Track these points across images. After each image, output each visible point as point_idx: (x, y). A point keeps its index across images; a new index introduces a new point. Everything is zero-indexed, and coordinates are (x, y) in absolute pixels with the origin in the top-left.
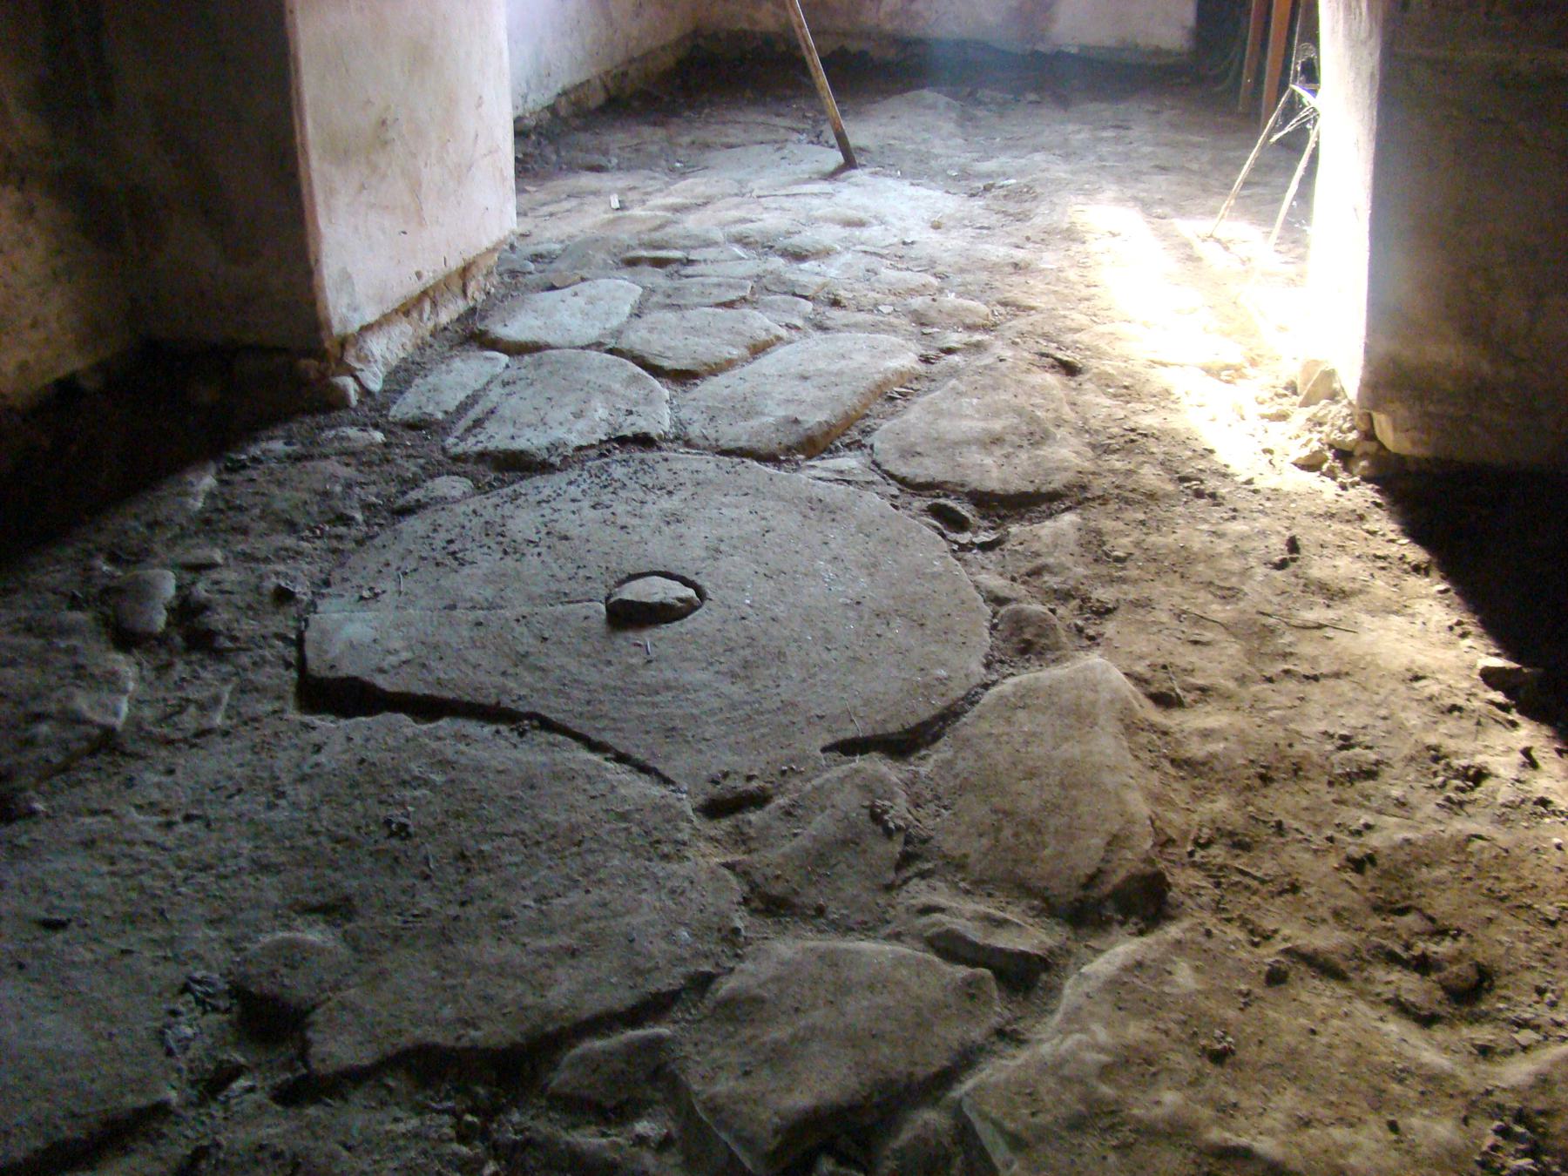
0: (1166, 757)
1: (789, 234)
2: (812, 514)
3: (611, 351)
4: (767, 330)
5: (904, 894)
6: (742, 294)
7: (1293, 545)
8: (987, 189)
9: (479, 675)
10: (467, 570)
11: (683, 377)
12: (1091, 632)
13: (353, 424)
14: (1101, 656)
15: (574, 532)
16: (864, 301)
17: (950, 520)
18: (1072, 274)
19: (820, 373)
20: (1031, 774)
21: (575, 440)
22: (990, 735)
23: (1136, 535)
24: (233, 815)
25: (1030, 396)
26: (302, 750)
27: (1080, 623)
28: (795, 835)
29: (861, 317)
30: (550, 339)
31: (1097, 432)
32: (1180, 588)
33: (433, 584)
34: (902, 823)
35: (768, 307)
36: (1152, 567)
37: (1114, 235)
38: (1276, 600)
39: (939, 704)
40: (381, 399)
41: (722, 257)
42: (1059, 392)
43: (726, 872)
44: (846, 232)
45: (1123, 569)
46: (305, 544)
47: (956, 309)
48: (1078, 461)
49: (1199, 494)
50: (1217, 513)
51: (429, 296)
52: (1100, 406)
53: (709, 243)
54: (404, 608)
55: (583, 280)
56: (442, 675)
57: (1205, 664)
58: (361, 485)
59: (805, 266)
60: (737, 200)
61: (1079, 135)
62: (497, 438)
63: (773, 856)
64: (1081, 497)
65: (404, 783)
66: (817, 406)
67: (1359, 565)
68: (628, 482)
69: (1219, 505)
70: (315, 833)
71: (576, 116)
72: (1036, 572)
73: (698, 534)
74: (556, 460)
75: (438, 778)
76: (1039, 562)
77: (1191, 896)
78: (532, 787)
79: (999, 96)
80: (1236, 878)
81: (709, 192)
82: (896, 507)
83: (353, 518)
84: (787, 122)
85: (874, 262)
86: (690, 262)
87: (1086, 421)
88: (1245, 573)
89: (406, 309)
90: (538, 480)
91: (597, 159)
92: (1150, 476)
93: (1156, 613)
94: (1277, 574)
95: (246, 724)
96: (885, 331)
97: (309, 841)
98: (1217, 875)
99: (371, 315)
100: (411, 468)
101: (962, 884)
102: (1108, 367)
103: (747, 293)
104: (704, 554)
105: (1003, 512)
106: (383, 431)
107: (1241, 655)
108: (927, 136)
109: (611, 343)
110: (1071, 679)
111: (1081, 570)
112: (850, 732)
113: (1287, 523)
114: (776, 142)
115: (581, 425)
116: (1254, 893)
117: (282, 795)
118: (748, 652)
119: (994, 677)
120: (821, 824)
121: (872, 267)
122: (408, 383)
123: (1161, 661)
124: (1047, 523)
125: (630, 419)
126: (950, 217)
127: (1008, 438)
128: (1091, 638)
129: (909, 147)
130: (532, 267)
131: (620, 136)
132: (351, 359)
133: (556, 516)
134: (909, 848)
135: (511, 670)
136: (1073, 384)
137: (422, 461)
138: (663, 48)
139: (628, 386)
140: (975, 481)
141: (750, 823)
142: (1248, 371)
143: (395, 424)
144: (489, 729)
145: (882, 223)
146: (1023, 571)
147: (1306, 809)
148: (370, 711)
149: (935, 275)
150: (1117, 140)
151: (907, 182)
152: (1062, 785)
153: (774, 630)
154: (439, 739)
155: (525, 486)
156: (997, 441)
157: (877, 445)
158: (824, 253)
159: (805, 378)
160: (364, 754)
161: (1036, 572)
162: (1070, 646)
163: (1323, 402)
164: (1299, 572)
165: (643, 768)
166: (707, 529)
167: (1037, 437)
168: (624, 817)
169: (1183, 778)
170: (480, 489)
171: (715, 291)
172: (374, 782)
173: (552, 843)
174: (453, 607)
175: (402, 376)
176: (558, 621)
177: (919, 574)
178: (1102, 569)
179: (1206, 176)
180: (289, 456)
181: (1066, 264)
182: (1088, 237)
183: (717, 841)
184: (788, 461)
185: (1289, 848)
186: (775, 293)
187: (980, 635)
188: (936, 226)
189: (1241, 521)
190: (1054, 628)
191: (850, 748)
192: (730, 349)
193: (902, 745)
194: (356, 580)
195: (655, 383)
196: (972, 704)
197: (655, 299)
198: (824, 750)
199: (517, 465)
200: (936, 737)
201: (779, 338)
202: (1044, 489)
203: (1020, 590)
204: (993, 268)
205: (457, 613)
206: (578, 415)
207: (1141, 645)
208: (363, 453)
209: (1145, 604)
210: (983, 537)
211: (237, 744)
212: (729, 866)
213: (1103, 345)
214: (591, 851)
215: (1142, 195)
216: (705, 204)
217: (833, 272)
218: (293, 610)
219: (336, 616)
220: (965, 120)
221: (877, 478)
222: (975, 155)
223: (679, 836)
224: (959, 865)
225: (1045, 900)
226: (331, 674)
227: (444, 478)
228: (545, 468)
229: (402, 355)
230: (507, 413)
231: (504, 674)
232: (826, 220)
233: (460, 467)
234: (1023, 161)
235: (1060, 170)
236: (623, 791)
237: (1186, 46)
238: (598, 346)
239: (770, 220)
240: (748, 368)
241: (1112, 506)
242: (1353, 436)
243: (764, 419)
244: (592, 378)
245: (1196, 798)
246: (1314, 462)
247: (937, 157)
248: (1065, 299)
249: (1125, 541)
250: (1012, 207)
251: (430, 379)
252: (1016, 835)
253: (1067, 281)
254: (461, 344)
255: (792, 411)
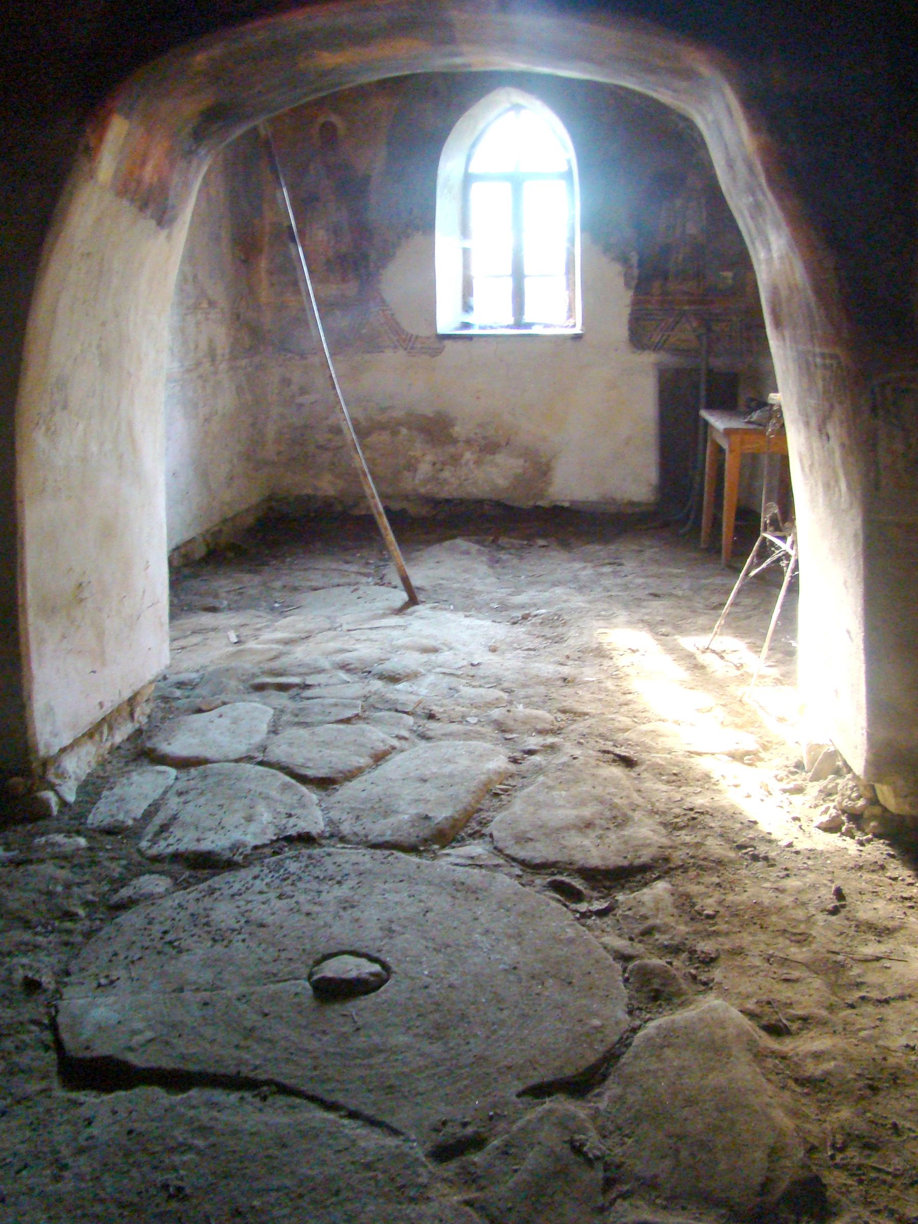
0: (790, 1077)
1: (381, 661)
2: (459, 895)
3: (261, 763)
4: (383, 741)
5: (613, 1214)
6: (356, 712)
7: (839, 894)
8: (525, 617)
9: (215, 1049)
10: (185, 957)
11: (325, 783)
12: (703, 978)
13: (59, 831)
14: (717, 998)
15: (269, 920)
16: (453, 715)
17: (570, 894)
18: (609, 684)
19: (435, 776)
20: (690, 1102)
21: (252, 841)
22: (648, 1071)
23: (717, 895)
24: (24, 1189)
25: (605, 787)
26: (76, 1124)
27: (693, 971)
28: (516, 1171)
29: (454, 727)
30: (209, 754)
31: (664, 813)
32: (763, 937)
33: (158, 971)
34: (598, 1153)
35: (379, 722)
36: (736, 920)
37: (634, 651)
38: (838, 940)
39: (601, 1048)
40: (77, 809)
41: (332, 681)
42: (626, 782)
43: (468, 1209)
44: (425, 657)
45: (715, 924)
46: (40, 939)
47: (527, 717)
48: (656, 838)
49: (755, 858)
50: (774, 873)
51: (108, 722)
52: (660, 791)
53: (321, 671)
54: (138, 993)
55: (224, 703)
56: (185, 1051)
57: (798, 997)
58: (79, 885)
59: (400, 686)
60: (331, 634)
61: (587, 573)
62: (184, 840)
63: (502, 1190)
64: (666, 868)
65: (172, 1150)
66: (441, 804)
67: (892, 906)
68: (303, 875)
69: (773, 865)
70: (102, 1201)
71: (185, 565)
72: (648, 932)
73: (372, 916)
74: (239, 858)
75: (200, 1143)
76: (650, 922)
77: (842, 1193)
78: (284, 1146)
79: (517, 542)
80: (873, 1175)
81: (310, 626)
82: (523, 885)
83: (76, 914)
84: (353, 568)
85: (454, 682)
86: (307, 687)
87: (653, 805)
88: (809, 919)
89: (90, 734)
90: (227, 876)
91: (210, 601)
92: (715, 847)
93: (749, 958)
94: (833, 918)
95: (19, 1102)
96: (475, 738)
97: (98, 1208)
98: (857, 1172)
99: (66, 740)
100: (116, 869)
101: (658, 1201)
102: (658, 758)
103: (358, 711)
104: (380, 934)
105: (608, 884)
106: (85, 836)
107: (824, 988)
108: (467, 576)
109: (260, 757)
110: (701, 1020)
111: (682, 928)
112: (535, 1078)
113: (829, 877)
114: (349, 584)
115: (253, 828)
116: (891, 1186)
117: (64, 1167)
118: (437, 1016)
119: (638, 1022)
120: (533, 1159)
121: (453, 685)
122: (98, 795)
123: (765, 998)
124: (645, 890)
125: (292, 821)
126: (502, 641)
127: (597, 822)
128: (705, 984)
129: (455, 586)
130: (178, 693)
131: (224, 582)
132: (51, 777)
133: (249, 906)
134: (609, 1174)
135: (242, 1043)
136: (633, 774)
137: (124, 862)
138: (248, 510)
139: (282, 793)
140: (580, 858)
141: (474, 1164)
142: (763, 755)
143: (94, 830)
144: (234, 1097)
145: (451, 649)
146: (636, 931)
147: (911, 1111)
148: (129, 1085)
149: (503, 690)
150: (615, 574)
151: (461, 614)
152: (719, 1110)
153: (454, 995)
154: (194, 1107)
155: (217, 881)
156: (589, 825)
157: (495, 834)
158: (412, 676)
159: (425, 781)
160: (130, 1125)
161: (648, 932)
162: (690, 991)
163: (831, 777)
164: (850, 915)
165: (372, 1122)
166: (377, 911)
167: (619, 820)
168: (368, 1166)
169: (807, 1094)
170: (180, 885)
171: (334, 710)
172: (145, 1150)
173: (313, 1194)
174: (181, 990)
175: (92, 788)
176: (274, 998)
177: (556, 939)
178: (699, 926)
179: (690, 600)
180: (11, 861)
181: (602, 676)
182: (614, 653)
183: (451, 1181)
184: (426, 851)
185: (907, 1146)
186: (381, 710)
187: (618, 988)
188: (493, 650)
189: (794, 878)
190: (674, 977)
191: (540, 1091)
192: (357, 758)
193: (581, 1085)
194: (93, 969)
195: (303, 789)
196: (628, 1046)
197: (285, 718)
198: (519, 1095)
199: (204, 864)
200: (605, 1077)
201: (394, 748)
202: (637, 862)
203: (639, 948)
204: (547, 682)
205: (187, 995)
206: (249, 819)
207: (746, 986)
208: (72, 857)
209: (738, 952)
210: (597, 906)
211: (14, 1123)
212: (468, 1203)
213: (647, 740)
214: (348, 1199)
215: (646, 617)
216: (307, 637)
217: (423, 691)
218: (43, 998)
219: (81, 1001)
220: (494, 562)
221: (501, 861)
222: (509, 591)
223: (421, 1180)
224: (650, 1185)
225: (731, 1208)
226: (88, 1055)
227: (147, 877)
228: (230, 865)
229: (89, 771)
230: (188, 819)
231: (237, 1046)
232: (407, 648)
233: (158, 866)
234: (547, 594)
235: (578, 601)
236: (363, 1144)
237: (652, 498)
238: (249, 759)
239: (364, 650)
240: (376, 773)
241: (692, 873)
242: (861, 803)
243: (401, 817)
244: (252, 786)
245: (822, 1110)
246: (833, 824)
247: (480, 593)
248: (608, 705)
249: (710, 901)
250: (547, 631)
251: (116, 790)
252: (693, 1155)
253: (606, 690)
254: (134, 760)
255: (421, 809)
